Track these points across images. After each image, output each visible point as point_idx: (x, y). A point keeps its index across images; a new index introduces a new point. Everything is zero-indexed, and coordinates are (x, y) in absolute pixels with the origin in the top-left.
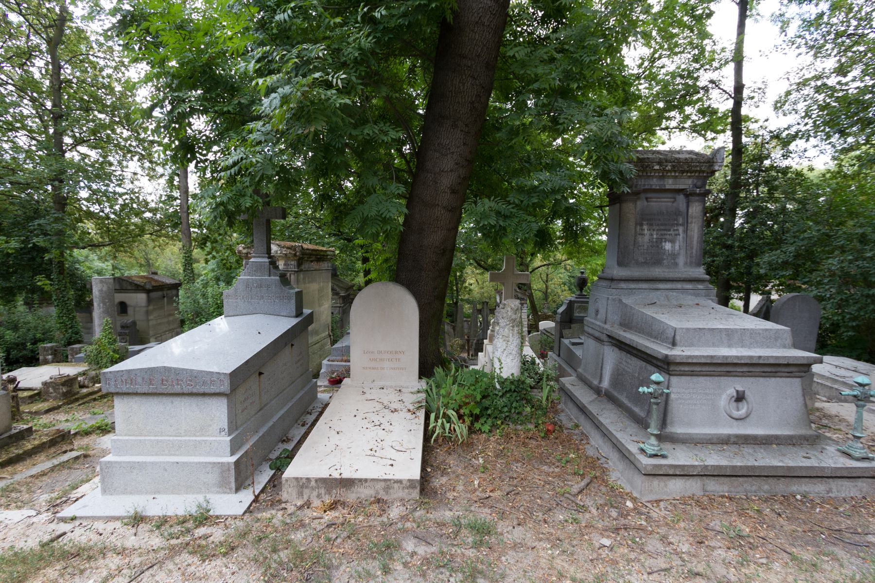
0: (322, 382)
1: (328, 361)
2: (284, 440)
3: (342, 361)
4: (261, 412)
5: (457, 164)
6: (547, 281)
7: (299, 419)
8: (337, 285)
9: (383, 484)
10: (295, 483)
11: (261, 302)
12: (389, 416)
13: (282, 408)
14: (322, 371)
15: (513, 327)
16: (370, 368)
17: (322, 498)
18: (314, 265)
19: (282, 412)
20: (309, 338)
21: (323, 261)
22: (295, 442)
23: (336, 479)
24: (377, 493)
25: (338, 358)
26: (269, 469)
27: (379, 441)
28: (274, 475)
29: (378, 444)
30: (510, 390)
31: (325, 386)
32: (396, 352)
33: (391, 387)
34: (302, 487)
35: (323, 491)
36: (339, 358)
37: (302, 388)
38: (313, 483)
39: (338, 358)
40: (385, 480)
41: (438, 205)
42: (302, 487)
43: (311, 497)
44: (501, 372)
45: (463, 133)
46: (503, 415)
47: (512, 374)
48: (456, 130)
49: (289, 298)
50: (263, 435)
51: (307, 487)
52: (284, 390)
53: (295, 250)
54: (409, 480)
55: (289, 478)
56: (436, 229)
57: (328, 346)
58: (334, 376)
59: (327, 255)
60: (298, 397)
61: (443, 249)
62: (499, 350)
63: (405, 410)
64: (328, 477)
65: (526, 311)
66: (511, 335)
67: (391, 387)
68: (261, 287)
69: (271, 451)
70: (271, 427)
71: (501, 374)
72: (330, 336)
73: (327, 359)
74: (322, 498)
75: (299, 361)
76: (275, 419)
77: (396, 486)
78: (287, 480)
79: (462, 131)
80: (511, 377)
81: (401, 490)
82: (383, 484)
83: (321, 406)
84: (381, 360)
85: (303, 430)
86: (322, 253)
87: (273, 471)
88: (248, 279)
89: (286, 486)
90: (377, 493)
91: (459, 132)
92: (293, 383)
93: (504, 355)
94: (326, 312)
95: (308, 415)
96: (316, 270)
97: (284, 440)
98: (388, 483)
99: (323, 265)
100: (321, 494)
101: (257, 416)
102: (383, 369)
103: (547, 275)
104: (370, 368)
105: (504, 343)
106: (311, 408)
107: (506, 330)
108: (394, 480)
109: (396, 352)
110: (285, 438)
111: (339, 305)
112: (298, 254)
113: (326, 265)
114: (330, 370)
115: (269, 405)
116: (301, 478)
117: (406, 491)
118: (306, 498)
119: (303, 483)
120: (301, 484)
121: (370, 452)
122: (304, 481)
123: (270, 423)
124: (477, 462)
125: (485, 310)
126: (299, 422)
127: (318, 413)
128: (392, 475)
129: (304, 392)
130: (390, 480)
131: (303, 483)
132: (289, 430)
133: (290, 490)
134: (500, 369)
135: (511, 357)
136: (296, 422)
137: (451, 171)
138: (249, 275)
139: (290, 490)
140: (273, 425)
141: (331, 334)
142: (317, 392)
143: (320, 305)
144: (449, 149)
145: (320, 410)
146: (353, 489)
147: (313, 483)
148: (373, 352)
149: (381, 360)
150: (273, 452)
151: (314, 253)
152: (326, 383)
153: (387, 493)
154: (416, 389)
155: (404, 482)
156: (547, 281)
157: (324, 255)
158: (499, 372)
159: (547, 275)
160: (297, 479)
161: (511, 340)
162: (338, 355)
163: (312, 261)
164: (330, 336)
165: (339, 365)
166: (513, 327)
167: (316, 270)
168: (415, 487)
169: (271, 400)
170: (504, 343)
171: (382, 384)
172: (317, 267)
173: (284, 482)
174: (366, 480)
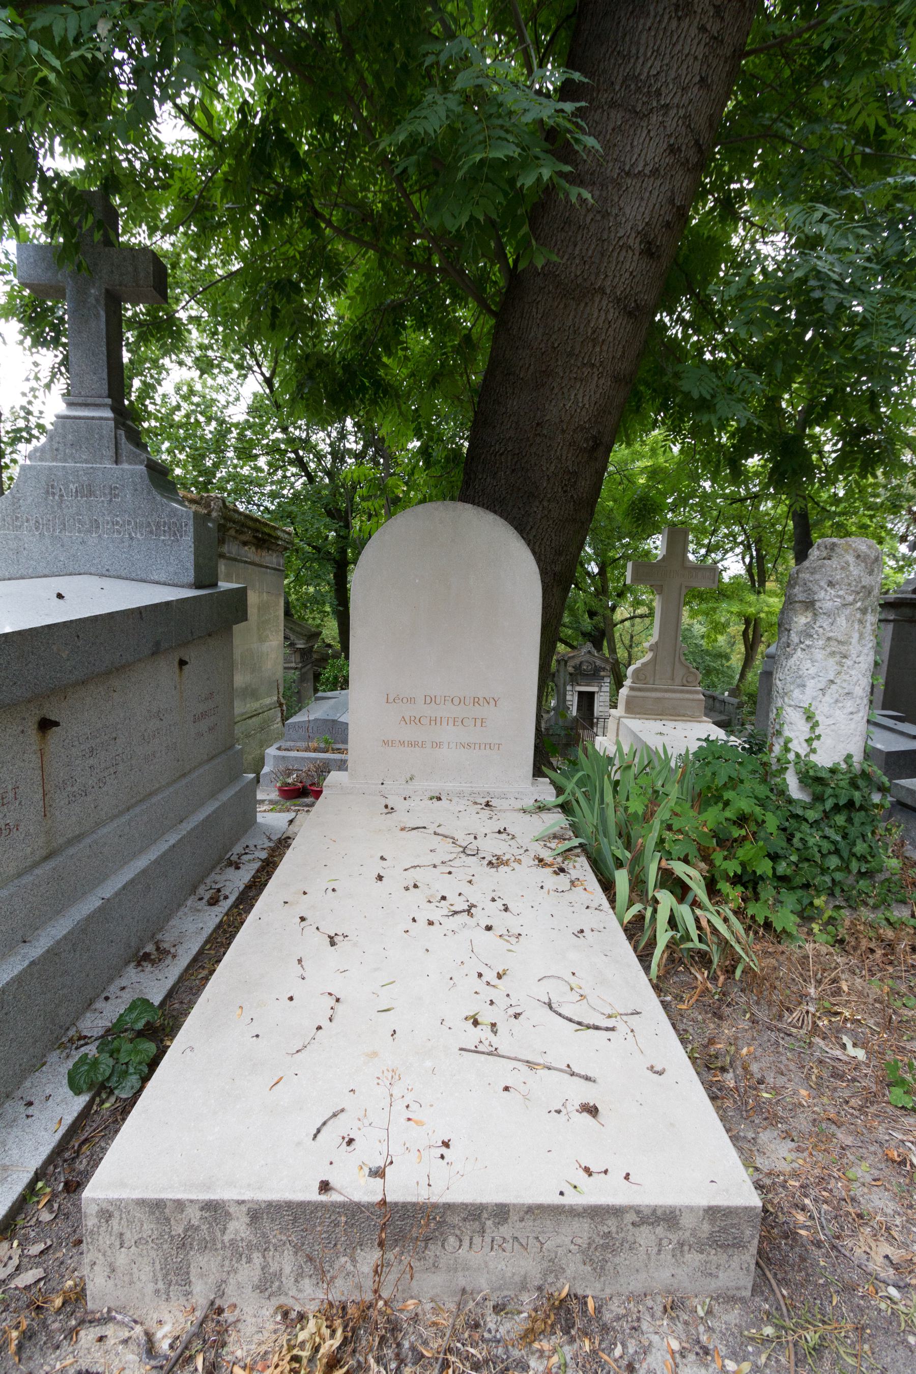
0: (267, 793)
1: (279, 749)
2: (146, 957)
3: (307, 749)
4: (52, 864)
5: (673, 150)
6: (631, 646)
7: (201, 881)
8: (291, 629)
9: (582, 1230)
10: (149, 1227)
11: (93, 539)
12: (488, 879)
13: (142, 851)
14: (266, 769)
15: (864, 611)
16: (402, 743)
17: (280, 1291)
18: (250, 553)
19: (141, 863)
20: (237, 703)
21: (269, 549)
22: (183, 961)
23: (353, 1210)
24: (554, 1269)
25: (299, 744)
26: (65, 1090)
27: (490, 976)
28: (85, 1114)
29: (492, 994)
30: (850, 804)
31: (271, 802)
32: (476, 701)
33: (460, 795)
34: (183, 1245)
35: (286, 1262)
36: (303, 744)
37: (213, 795)
38: (238, 1227)
39: (299, 744)
40: (596, 1213)
41: (602, 290)
42: (183, 1245)
43: (230, 1290)
44: (813, 751)
45: (705, 38)
46: (827, 879)
47: (849, 757)
48: (685, 24)
49: (175, 531)
50: (52, 953)
51: (206, 1246)
52: (151, 794)
53: (207, 505)
54: (712, 1212)
55: (118, 1204)
56: (586, 371)
57: (277, 725)
58: (290, 781)
59: (277, 538)
60: (201, 815)
61: (594, 438)
62: (810, 684)
63: (528, 860)
64: (313, 1195)
65: (608, 689)
66: (856, 636)
67: (460, 795)
68: (91, 493)
69: (91, 1002)
70: (89, 918)
71: (813, 758)
72: (281, 705)
73: (276, 745)
74: (280, 1291)
75: (204, 715)
76: (109, 889)
77: (645, 1237)
78: (106, 1215)
79: (702, 29)
80: (844, 766)
81: (666, 1257)
82: (582, 1230)
83: (268, 844)
84: (434, 721)
85: (212, 918)
86: (266, 530)
87: (84, 1099)
88: (50, 468)
89: (105, 1240)
90: (554, 1269)
91: (694, 31)
92: (184, 775)
93: (827, 699)
94: (273, 656)
95: (231, 870)
96: (252, 563)
97: (146, 957)
98: (611, 1224)
99: (268, 558)
100: (278, 1275)
101: (28, 879)
102: (439, 745)
103: (632, 637)
104: (402, 743)
105: (832, 661)
106: (238, 849)
107: (842, 621)
108: (637, 1210)
109: (476, 701)
110: (150, 948)
111: (293, 665)
112: (214, 514)
113: (275, 560)
114: (281, 768)
115: (88, 841)
116: (180, 1205)
117: (693, 1258)
118: (201, 1293)
119: (190, 1228)
120: (179, 1230)
121: (473, 1035)
122: (194, 1215)
123: (90, 904)
124: (838, 1053)
125: (562, 674)
126: (201, 890)
127: (257, 865)
128: (616, 1176)
129: (217, 804)
130: (617, 1212)
131: (190, 1228)
132: (168, 918)
133: (122, 1259)
134: (809, 741)
135: (849, 705)
136: (194, 890)
137: (655, 172)
138: (54, 459)
139: (122, 1259)
140: (100, 909)
141: (283, 701)
142: (255, 812)
143: (262, 639)
144: (658, 93)
145: (264, 855)
146: (434, 1250)
147: (238, 1227)
148: (412, 700)
149: (434, 721)
150: (99, 1004)
151: (250, 523)
152: (274, 795)
153: (600, 1269)
154: (529, 803)
155: (687, 1221)
156: (631, 646)
157: (269, 535)
158: (803, 750)
159: (632, 637)
160: (156, 1207)
161: (854, 653)
162: (301, 739)
163: (245, 544)
164: (281, 705)
165: (303, 758)
166: (864, 611)
167: (252, 563)
168: (739, 1245)
169: (99, 824)
170: (832, 661)
171: (435, 786)
172: (257, 559)
173: (91, 1222)
174: (501, 1212)
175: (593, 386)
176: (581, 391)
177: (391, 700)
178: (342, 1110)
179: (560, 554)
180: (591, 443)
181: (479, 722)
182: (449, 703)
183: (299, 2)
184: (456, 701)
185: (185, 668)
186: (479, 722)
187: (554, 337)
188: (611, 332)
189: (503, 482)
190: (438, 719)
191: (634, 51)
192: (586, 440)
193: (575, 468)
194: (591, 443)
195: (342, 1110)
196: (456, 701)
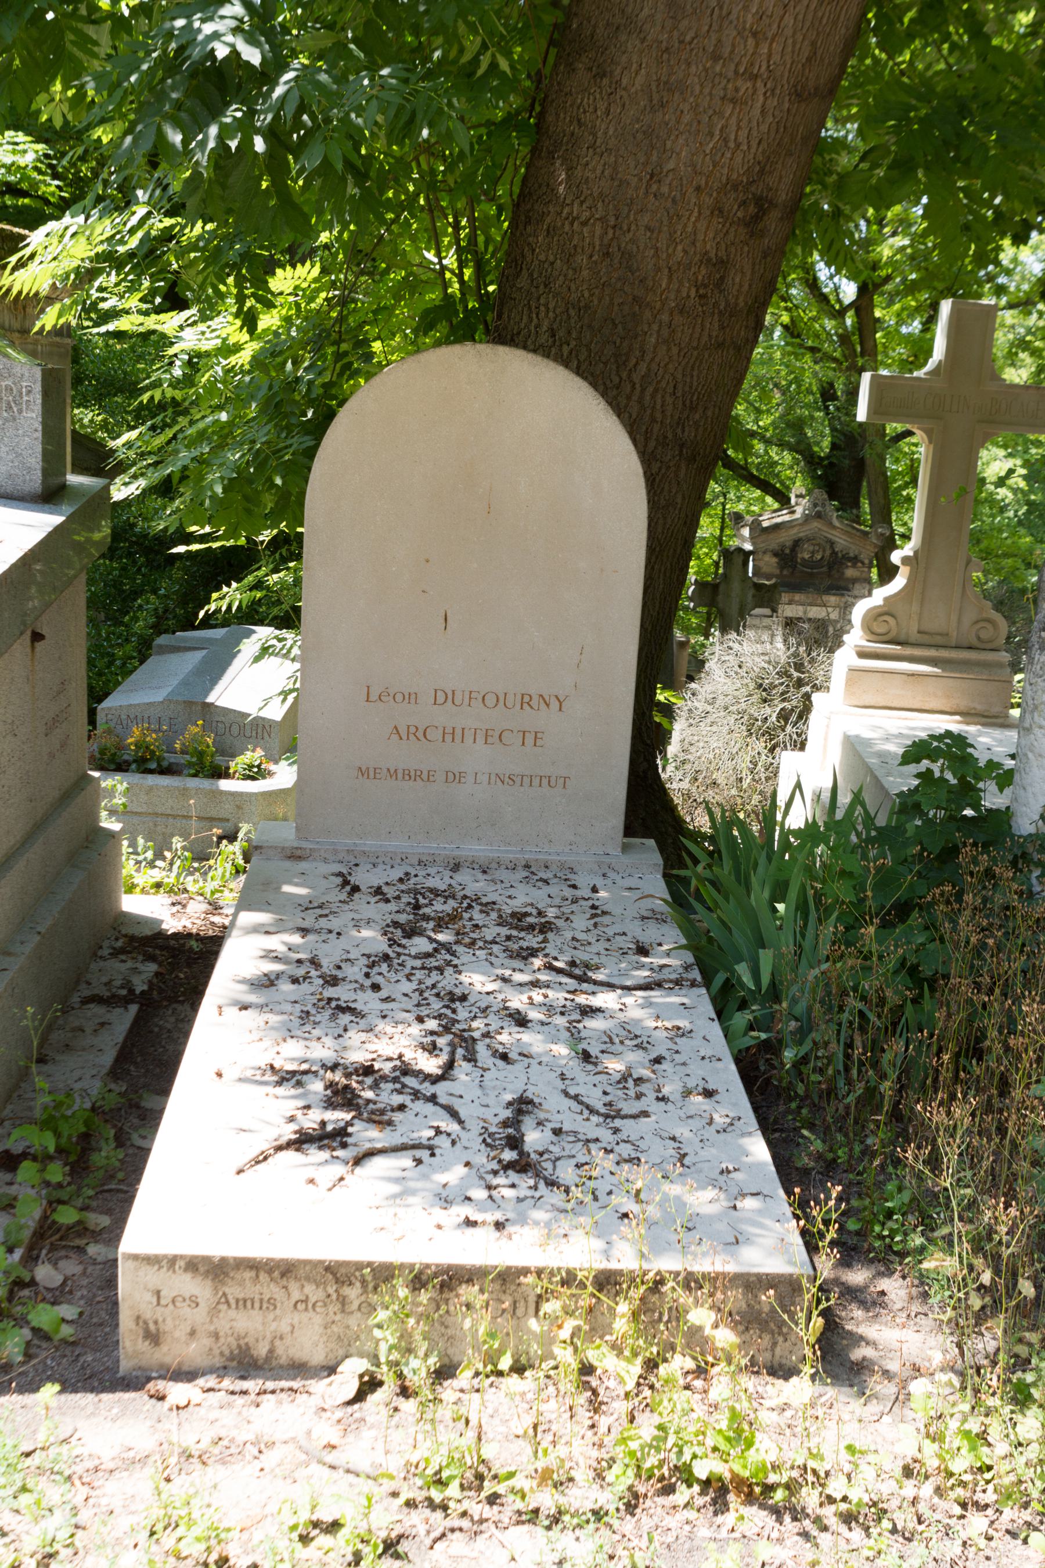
84: (450, 734)
109: (526, 700)
148: (411, 698)
175: (756, 112)
176: (733, 121)
177: (374, 697)
178: (330, 1190)
179: (693, 409)
180: (752, 209)
181: (530, 739)
182: (477, 704)
183: (11, 31)
184: (491, 700)
185: (40, 646)
186: (530, 739)
187: (685, 23)
188: (789, 20)
189: (585, 273)
190: (458, 732)
191: (737, 280)
192: (744, 203)
193: (722, 253)
194: (752, 209)
195: (330, 1190)
196: (491, 700)
